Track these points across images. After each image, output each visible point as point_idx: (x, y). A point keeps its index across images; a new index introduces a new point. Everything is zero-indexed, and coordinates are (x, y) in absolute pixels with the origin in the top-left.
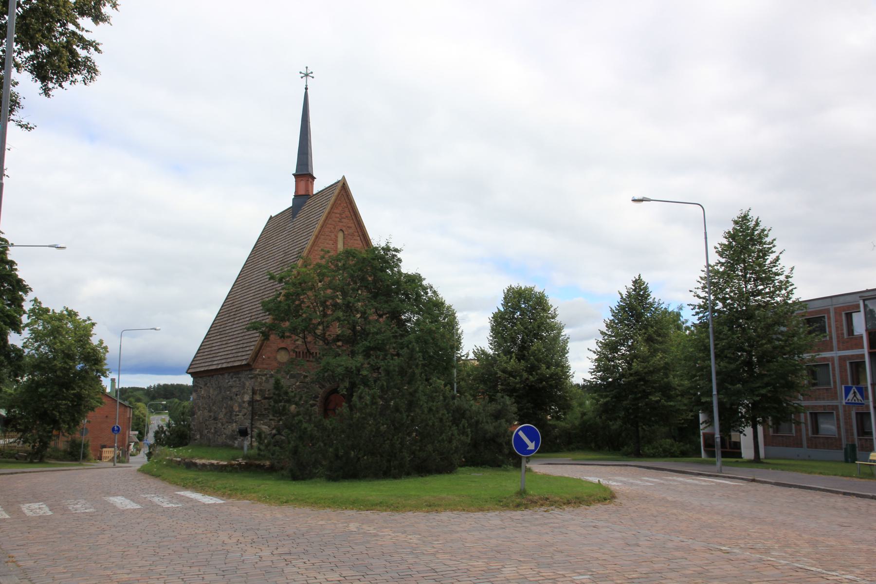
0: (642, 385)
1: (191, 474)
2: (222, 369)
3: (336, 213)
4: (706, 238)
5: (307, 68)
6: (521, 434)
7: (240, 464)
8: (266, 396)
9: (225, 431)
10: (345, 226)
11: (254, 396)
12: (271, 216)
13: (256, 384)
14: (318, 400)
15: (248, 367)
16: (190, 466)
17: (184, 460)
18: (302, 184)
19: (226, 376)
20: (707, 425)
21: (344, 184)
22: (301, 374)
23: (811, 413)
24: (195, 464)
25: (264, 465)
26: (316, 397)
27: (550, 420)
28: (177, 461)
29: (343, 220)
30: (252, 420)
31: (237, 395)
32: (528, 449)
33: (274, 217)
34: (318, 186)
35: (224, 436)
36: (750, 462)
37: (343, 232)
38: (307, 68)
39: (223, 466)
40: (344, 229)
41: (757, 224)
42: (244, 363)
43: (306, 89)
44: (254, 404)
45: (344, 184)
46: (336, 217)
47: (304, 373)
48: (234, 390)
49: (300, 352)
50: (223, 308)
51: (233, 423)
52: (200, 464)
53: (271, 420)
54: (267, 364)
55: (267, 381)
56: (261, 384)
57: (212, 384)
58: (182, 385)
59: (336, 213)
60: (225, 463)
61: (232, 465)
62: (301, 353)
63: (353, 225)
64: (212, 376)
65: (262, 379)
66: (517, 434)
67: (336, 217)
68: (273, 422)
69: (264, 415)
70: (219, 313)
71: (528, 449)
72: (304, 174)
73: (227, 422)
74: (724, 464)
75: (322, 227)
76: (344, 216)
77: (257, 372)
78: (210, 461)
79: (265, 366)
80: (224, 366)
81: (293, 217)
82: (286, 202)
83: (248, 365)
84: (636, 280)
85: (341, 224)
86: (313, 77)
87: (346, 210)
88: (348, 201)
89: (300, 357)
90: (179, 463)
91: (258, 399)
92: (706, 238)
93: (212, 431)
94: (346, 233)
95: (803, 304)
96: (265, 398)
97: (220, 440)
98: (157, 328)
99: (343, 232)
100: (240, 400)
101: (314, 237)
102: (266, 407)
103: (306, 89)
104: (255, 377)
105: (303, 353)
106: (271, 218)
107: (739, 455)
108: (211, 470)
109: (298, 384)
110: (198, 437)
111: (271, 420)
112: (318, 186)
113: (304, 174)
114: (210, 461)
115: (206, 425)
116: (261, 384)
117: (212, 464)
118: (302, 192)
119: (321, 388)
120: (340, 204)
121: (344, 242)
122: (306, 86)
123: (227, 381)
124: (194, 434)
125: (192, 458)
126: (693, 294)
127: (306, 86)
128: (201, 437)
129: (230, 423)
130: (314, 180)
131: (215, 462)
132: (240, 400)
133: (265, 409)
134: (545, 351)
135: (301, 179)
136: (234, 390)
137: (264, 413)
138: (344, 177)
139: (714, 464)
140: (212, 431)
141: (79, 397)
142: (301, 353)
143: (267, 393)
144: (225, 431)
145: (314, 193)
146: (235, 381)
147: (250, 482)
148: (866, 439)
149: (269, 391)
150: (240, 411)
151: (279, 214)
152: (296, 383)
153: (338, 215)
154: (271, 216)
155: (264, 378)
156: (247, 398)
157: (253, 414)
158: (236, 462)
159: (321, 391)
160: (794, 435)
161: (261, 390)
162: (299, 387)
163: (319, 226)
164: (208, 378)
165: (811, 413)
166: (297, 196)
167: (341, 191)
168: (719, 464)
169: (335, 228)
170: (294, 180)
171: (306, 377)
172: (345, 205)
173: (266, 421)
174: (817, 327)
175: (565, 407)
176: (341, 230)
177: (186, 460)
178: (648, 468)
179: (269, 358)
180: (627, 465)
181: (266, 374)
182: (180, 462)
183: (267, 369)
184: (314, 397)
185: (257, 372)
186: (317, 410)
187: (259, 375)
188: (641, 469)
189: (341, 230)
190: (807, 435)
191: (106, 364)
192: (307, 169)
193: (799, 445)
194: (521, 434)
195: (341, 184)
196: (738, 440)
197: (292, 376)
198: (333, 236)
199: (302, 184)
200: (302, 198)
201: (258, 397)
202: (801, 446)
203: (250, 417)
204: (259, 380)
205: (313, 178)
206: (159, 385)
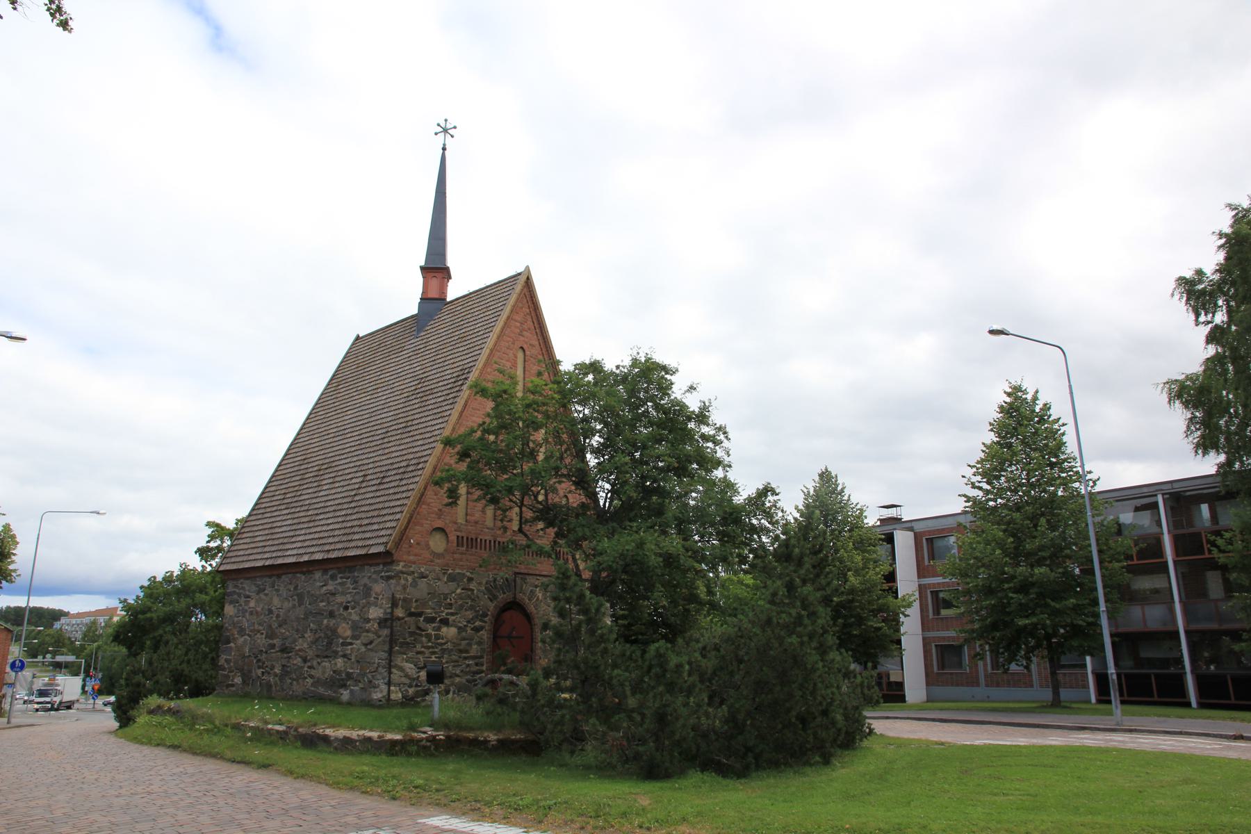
1: (305, 758)
2: (367, 556)
3: (516, 321)
4: (1071, 393)
7: (433, 739)
8: (413, 610)
9: (313, 672)
10: (526, 343)
11: (395, 610)
12: (358, 336)
13: (398, 588)
14: (486, 619)
15: (386, 558)
16: (312, 741)
17: (296, 730)
18: (434, 283)
19: (318, 575)
21: (528, 278)
22: (464, 574)
23: (936, 646)
24: (325, 739)
25: (486, 742)
26: (485, 615)
28: (278, 732)
29: (525, 333)
30: (390, 652)
31: (346, 608)
34: (454, 291)
35: (309, 681)
36: (919, 707)
37: (524, 351)
39: (394, 743)
40: (525, 347)
41: (1035, 398)
42: (381, 549)
43: (444, 149)
44: (394, 624)
45: (528, 278)
46: (516, 327)
47: (468, 574)
48: (339, 599)
49: (463, 537)
50: (281, 468)
51: (336, 658)
52: (336, 739)
53: (418, 653)
54: (416, 555)
55: (414, 584)
56: (405, 587)
57: (278, 590)
58: (41, 608)
59: (516, 321)
60: (398, 737)
61: (412, 741)
62: (465, 539)
63: (537, 343)
64: (279, 576)
65: (407, 580)
67: (516, 327)
68: (421, 657)
69: (408, 643)
70: (273, 476)
72: (435, 269)
73: (318, 656)
74: (1124, 713)
75: (498, 338)
76: (525, 326)
77: (400, 567)
78: (361, 733)
79: (412, 558)
80: (319, 557)
81: (419, 331)
82: (409, 306)
83: (388, 554)
84: (823, 473)
85: (522, 338)
87: (529, 318)
88: (531, 305)
89: (463, 546)
90: (283, 736)
91: (401, 615)
92: (1071, 393)
93: (277, 671)
94: (527, 353)
96: (411, 614)
97: (297, 688)
98: (101, 512)
99: (524, 351)
100: (355, 617)
101: (488, 351)
102: (413, 629)
103: (444, 149)
104: (397, 576)
105: (467, 538)
106: (358, 338)
107: (901, 698)
108: (367, 752)
109: (459, 591)
110: (238, 680)
111: (418, 653)
112: (454, 291)
113: (435, 269)
114: (361, 733)
115: (259, 661)
116: (405, 587)
117: (369, 739)
118: (433, 294)
119: (491, 601)
120: (522, 308)
121: (524, 367)
122: (444, 145)
123: (318, 583)
124: (227, 677)
125: (315, 725)
126: (965, 480)
127: (444, 145)
128: (244, 681)
129: (327, 657)
131: (374, 735)
132: (355, 617)
133: (412, 634)
135: (434, 274)
136: (339, 599)
137: (408, 640)
138: (527, 268)
139: (1110, 713)
140: (277, 671)
141: (989, 476)
142: (465, 539)
143: (414, 605)
144: (313, 672)
146: (342, 584)
147: (443, 772)
148: (1065, 673)
149: (416, 601)
150: (355, 637)
151: (495, 284)
152: (456, 589)
153: (518, 324)
154: (358, 336)
155: (410, 578)
156: (375, 613)
157: (392, 641)
158: (424, 736)
159: (491, 606)
160: (968, 671)
161: (405, 600)
162: (460, 597)
163: (495, 336)
164: (268, 579)
165: (936, 646)
166: (424, 299)
167: (524, 287)
168: (1119, 712)
169: (513, 344)
170: (422, 279)
171: (470, 580)
172: (528, 310)
173: (410, 654)
176: (522, 348)
177: (300, 730)
178: (933, 720)
179: (418, 544)
180: (888, 718)
181: (413, 573)
182: (285, 732)
183: (414, 563)
184: (481, 616)
185: (400, 567)
186: (485, 637)
187: (403, 573)
188: (921, 722)
189: (522, 348)
190: (985, 670)
191: (13, 562)
193: (974, 682)
195: (523, 279)
196: (900, 680)
197: (452, 578)
198: (511, 355)
200: (433, 302)
201: (400, 612)
202: (978, 685)
203: (386, 648)
204: (403, 582)
206: (8, 608)
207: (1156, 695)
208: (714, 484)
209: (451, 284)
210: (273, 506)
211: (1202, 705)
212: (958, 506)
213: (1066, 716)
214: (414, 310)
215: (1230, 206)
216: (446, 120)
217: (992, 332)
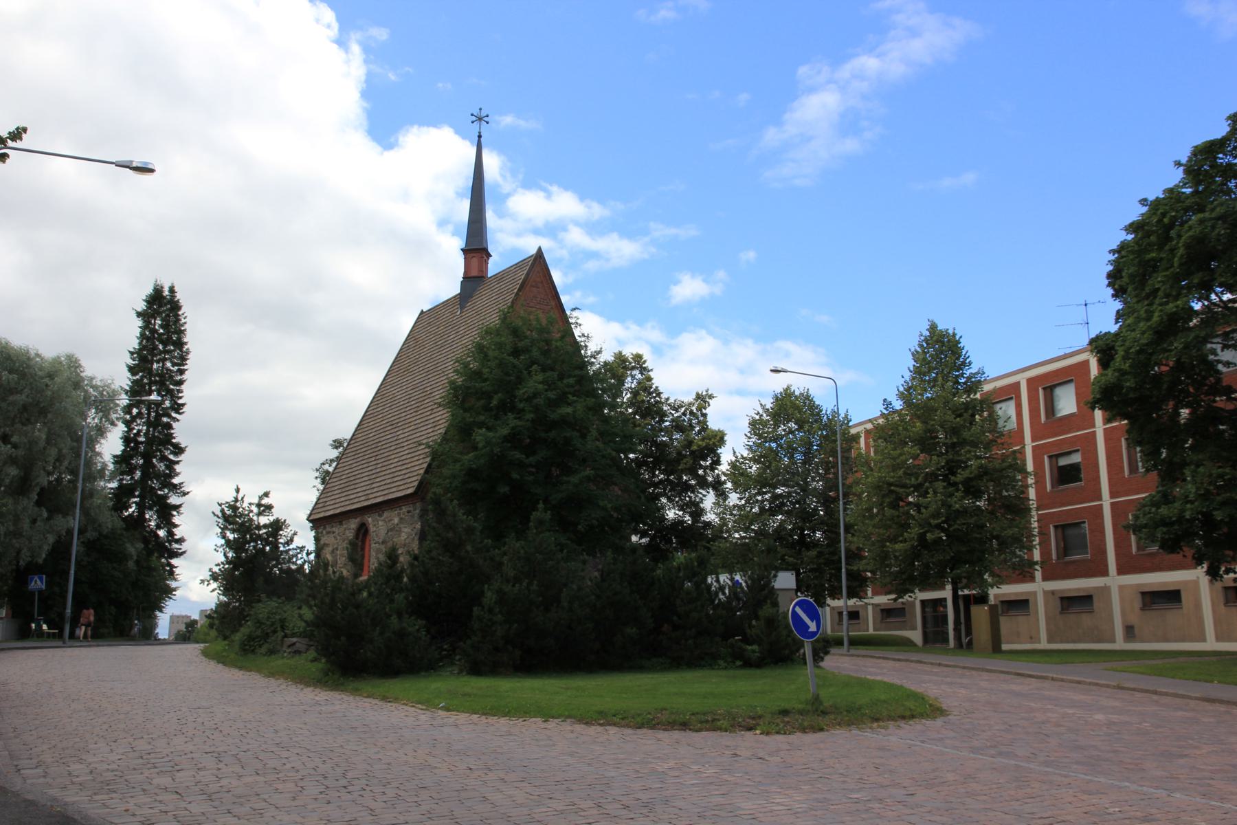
0: (1204, 401)
5: (480, 109)
6: (798, 609)
12: (422, 311)
18: (475, 262)
20: (22, 563)
27: (639, 420)
32: (810, 630)
33: (426, 312)
34: (495, 266)
38: (480, 109)
66: (794, 613)
71: (810, 630)
72: (476, 249)
82: (450, 286)
86: (487, 123)
95: (790, 568)
103: (480, 137)
106: (422, 312)
118: (474, 273)
122: (480, 133)
127: (480, 133)
130: (488, 259)
134: (804, 572)
135: (474, 255)
145: (489, 276)
154: (422, 311)
174: (1000, 451)
175: (348, 579)
192: (482, 243)
194: (798, 609)
199: (475, 262)
200: (474, 280)
205: (489, 255)
207: (1043, 635)
208: (723, 567)
209: (491, 261)
210: (373, 474)
211: (1105, 429)
212: (1228, 129)
213: (517, 679)
214: (456, 290)
215: (173, 284)
216: (472, 115)
217: (145, 170)
